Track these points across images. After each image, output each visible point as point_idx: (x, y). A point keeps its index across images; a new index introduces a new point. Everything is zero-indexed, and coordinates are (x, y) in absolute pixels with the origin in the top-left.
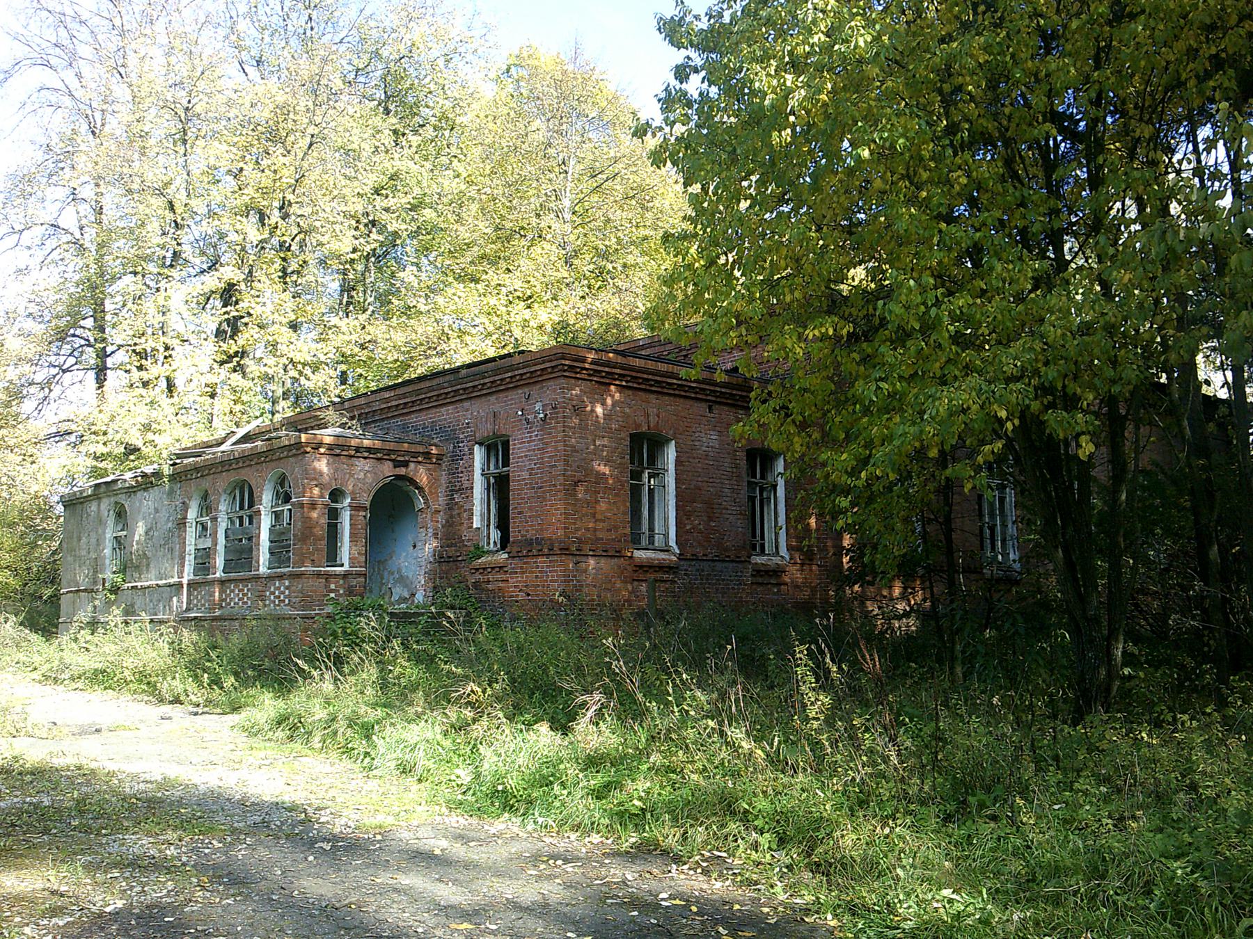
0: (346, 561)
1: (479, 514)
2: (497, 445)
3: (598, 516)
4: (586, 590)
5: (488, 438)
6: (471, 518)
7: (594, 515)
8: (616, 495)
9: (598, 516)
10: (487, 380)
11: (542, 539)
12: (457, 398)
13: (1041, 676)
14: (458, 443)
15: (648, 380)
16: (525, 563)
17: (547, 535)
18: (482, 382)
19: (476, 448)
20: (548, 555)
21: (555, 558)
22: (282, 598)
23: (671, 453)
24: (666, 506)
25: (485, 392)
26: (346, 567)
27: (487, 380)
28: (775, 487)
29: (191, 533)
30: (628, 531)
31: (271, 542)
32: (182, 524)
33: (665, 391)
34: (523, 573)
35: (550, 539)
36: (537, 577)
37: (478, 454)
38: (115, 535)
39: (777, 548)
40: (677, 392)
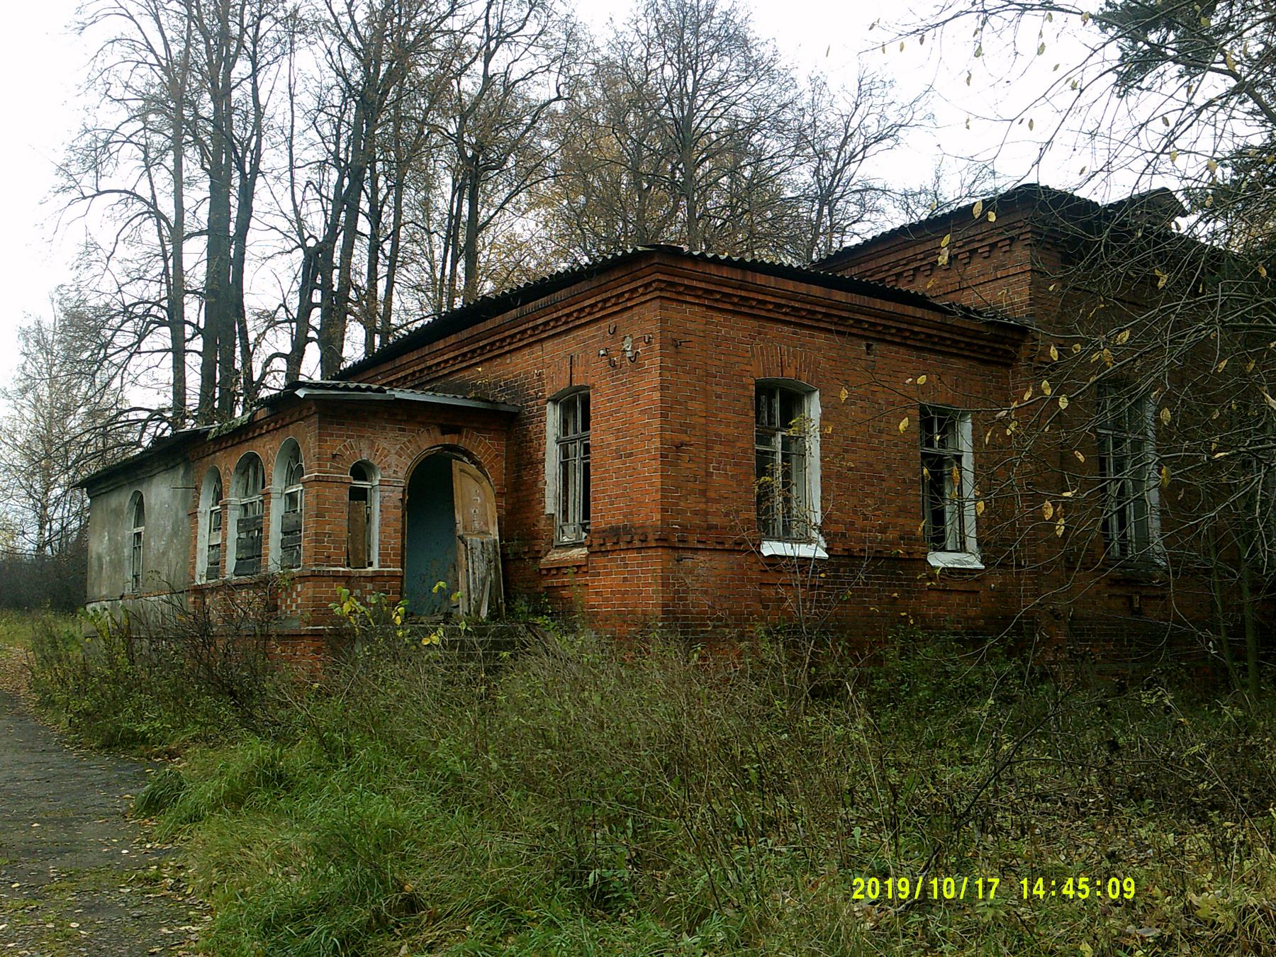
0: (375, 558)
1: (552, 495)
2: (1229, 641)
3: (712, 494)
4: (691, 597)
5: (563, 393)
6: (541, 501)
7: (703, 493)
8: (736, 464)
9: (712, 494)
10: (560, 313)
11: (632, 527)
12: (525, 342)
13: (1264, 720)
14: (527, 401)
15: (765, 302)
16: (610, 560)
17: (638, 520)
18: (555, 315)
19: (549, 406)
20: (639, 550)
21: (650, 553)
22: (294, 605)
23: (814, 408)
24: (384, 523)
25: (559, 330)
26: (376, 567)
27: (560, 313)
28: (959, 458)
29: (204, 523)
30: (753, 515)
31: (285, 533)
32: (193, 515)
33: (805, 322)
34: (610, 574)
35: (642, 527)
36: (625, 579)
37: (553, 416)
38: (136, 531)
39: (963, 543)
40: (474, 361)
